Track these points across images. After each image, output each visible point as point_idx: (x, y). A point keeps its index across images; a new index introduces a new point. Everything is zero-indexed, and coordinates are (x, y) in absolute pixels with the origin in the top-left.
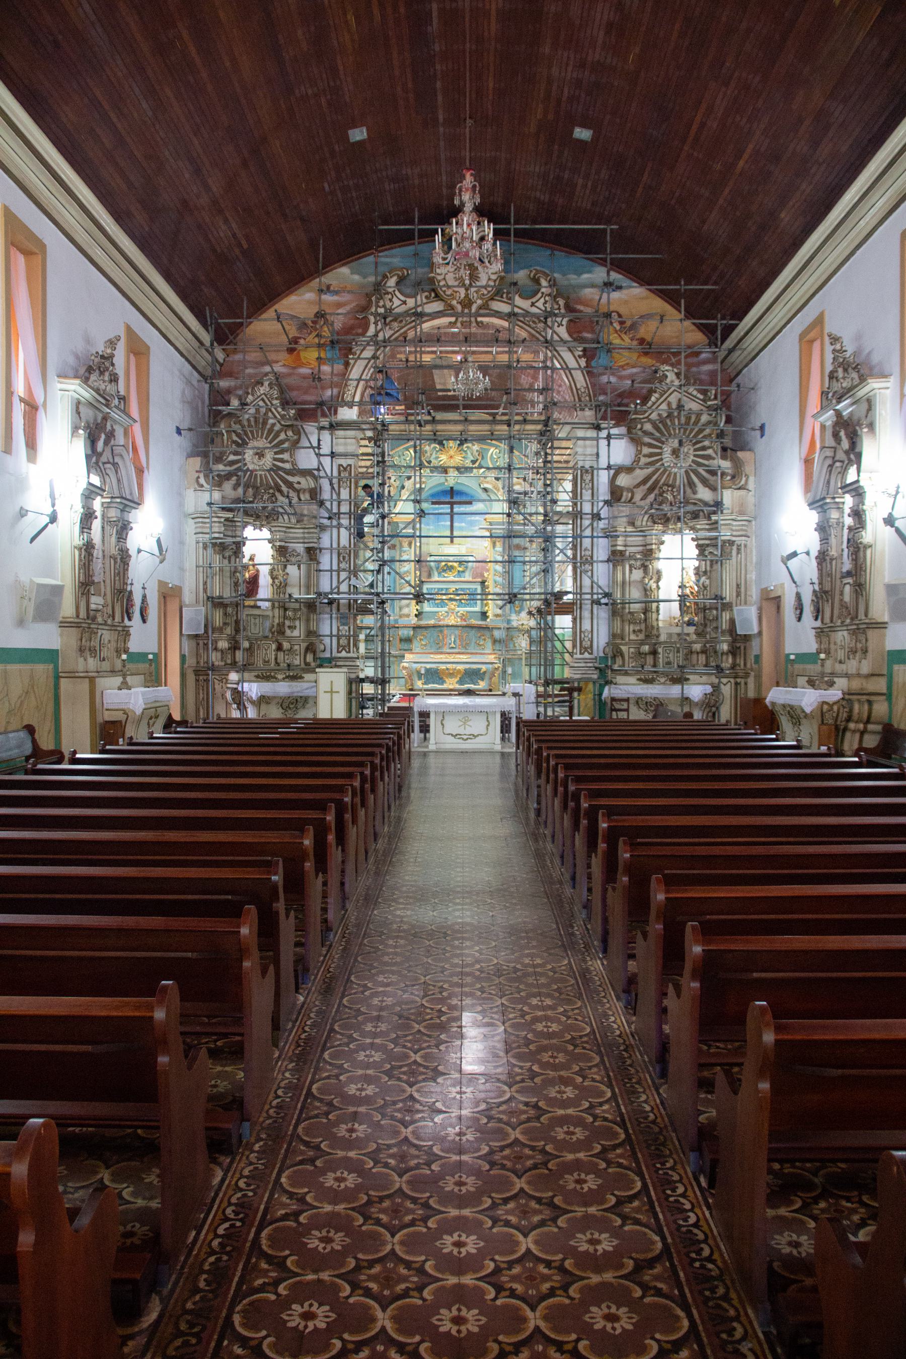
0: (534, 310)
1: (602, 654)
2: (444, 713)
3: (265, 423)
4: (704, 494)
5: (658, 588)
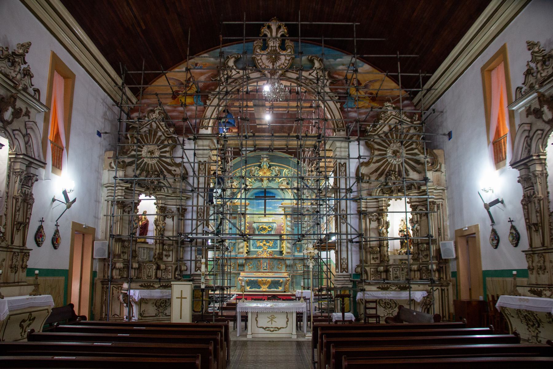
0: (311, 77)
1: (354, 273)
2: (257, 313)
3: (155, 135)
4: (414, 175)
5: (387, 232)
